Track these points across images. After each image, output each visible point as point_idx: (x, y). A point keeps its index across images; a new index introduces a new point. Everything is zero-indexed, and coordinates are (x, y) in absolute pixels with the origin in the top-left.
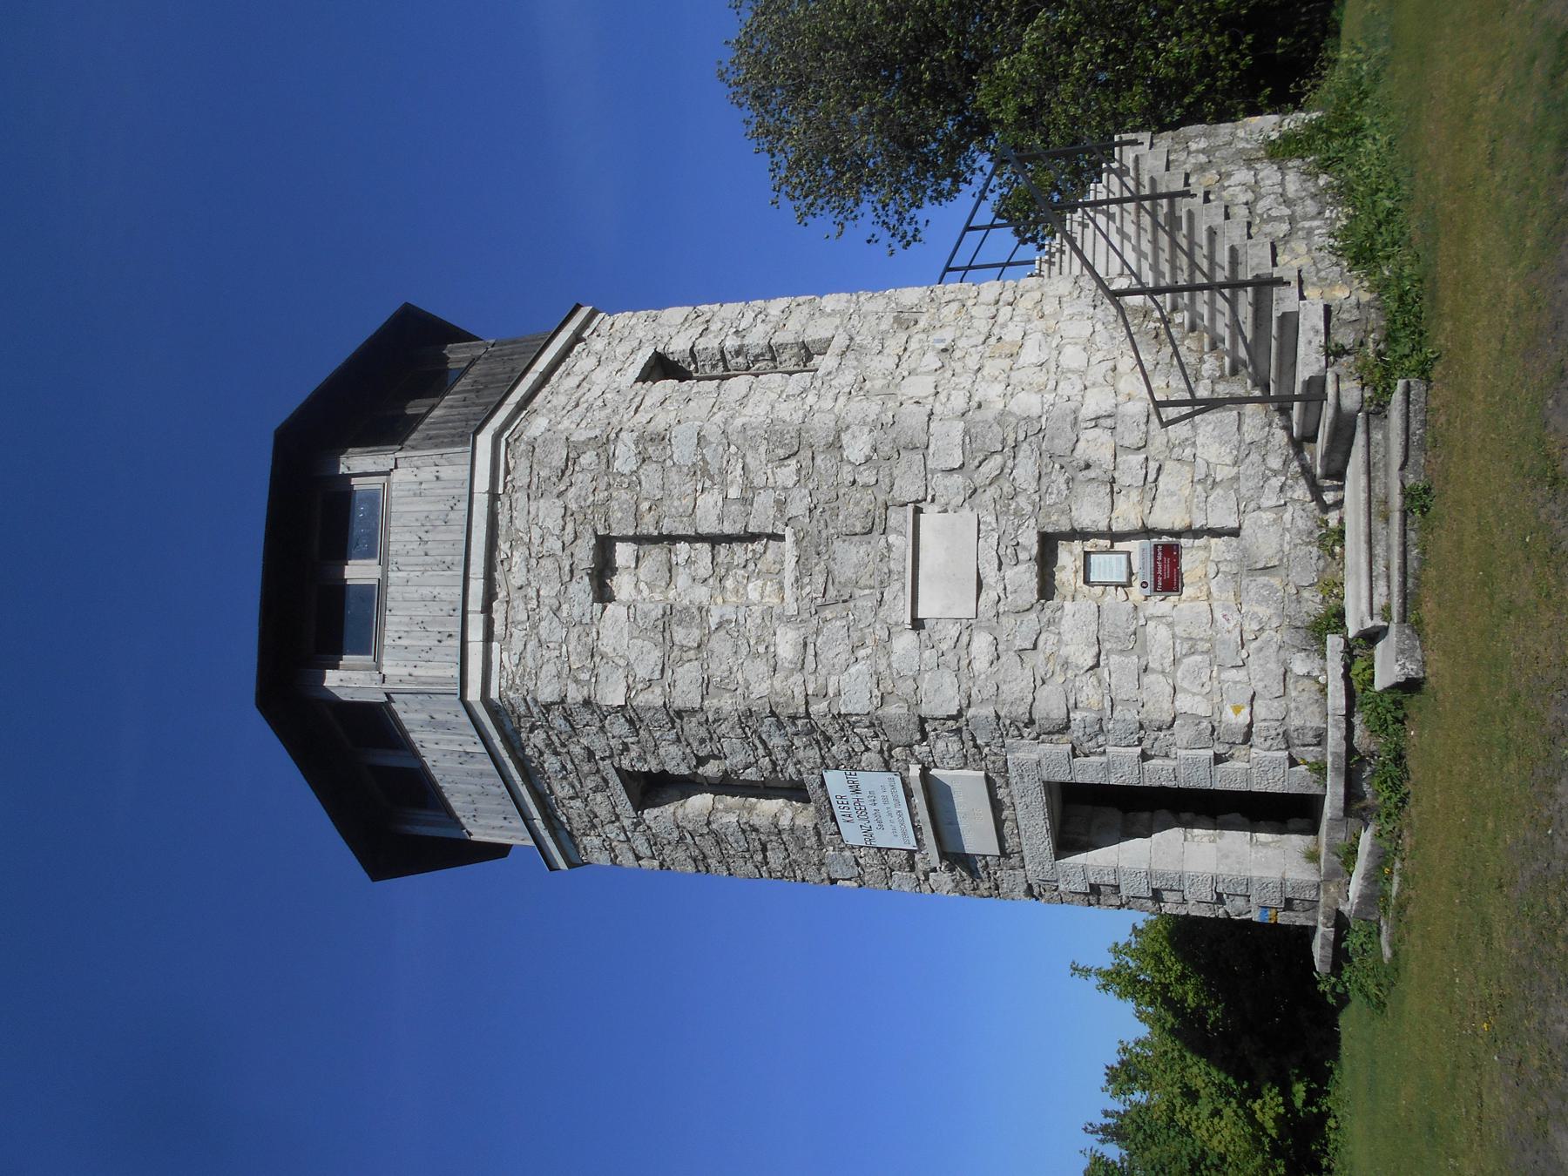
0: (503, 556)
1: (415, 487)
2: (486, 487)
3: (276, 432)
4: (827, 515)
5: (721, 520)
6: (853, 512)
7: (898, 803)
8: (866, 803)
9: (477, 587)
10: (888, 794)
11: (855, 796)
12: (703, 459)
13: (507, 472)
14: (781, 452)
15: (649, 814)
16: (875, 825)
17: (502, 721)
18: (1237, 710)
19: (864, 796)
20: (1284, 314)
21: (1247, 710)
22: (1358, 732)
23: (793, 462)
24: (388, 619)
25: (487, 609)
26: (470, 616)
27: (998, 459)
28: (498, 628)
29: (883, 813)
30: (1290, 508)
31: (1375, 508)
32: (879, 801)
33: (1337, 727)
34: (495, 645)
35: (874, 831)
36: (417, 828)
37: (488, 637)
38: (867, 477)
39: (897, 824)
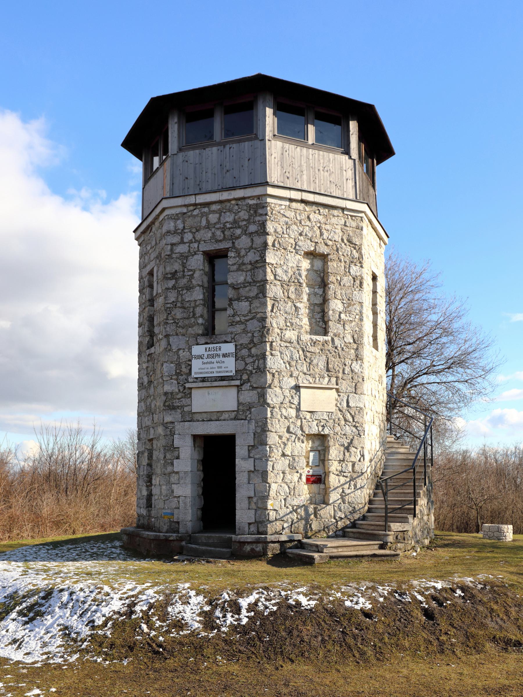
0: (321, 211)
1: (344, 169)
2: (348, 207)
3: (373, 106)
4: (334, 353)
5: (333, 310)
6: (335, 363)
7: (217, 372)
8: (217, 359)
9: (310, 197)
10: (223, 369)
11: (221, 355)
12: (354, 304)
13: (351, 216)
14: (356, 336)
15: (200, 257)
16: (205, 361)
17: (253, 199)
18: (272, 505)
19: (222, 359)
20: (408, 518)
21: (272, 508)
22: (272, 545)
23: (352, 341)
24: (293, 146)
25: (302, 201)
26: (300, 193)
27: (351, 420)
28: (294, 205)
29: (212, 365)
30: (335, 521)
31: (494, 543)
32: (219, 365)
33: (275, 538)
34: (287, 203)
35: (201, 360)
36: (176, 126)
37: (291, 200)
38: (347, 370)
39: (206, 370)
